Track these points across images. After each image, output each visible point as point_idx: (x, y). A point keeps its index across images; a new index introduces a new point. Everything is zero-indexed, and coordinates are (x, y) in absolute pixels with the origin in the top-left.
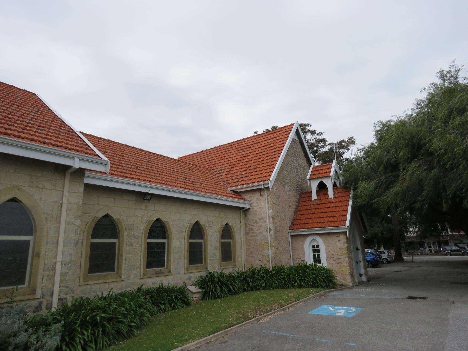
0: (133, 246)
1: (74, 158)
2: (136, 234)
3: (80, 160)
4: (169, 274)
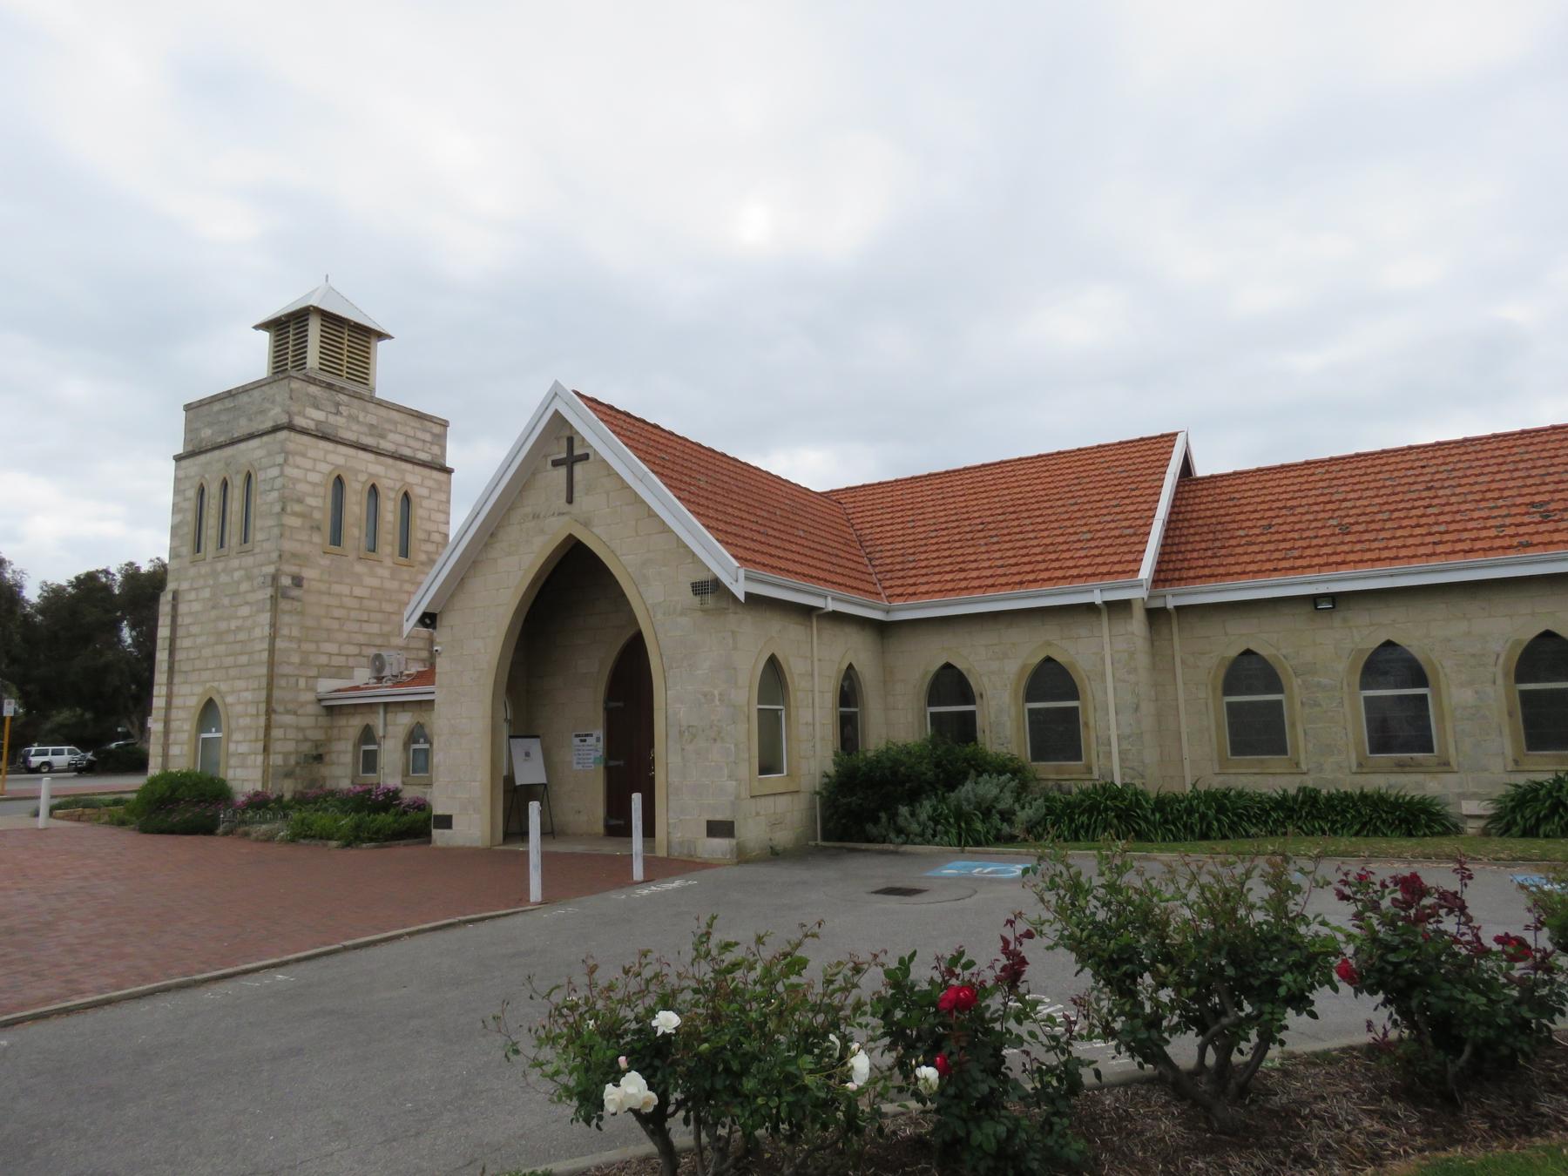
0: (1320, 705)
1: (826, 597)
2: (1324, 681)
3: (833, 599)
4: (1446, 768)
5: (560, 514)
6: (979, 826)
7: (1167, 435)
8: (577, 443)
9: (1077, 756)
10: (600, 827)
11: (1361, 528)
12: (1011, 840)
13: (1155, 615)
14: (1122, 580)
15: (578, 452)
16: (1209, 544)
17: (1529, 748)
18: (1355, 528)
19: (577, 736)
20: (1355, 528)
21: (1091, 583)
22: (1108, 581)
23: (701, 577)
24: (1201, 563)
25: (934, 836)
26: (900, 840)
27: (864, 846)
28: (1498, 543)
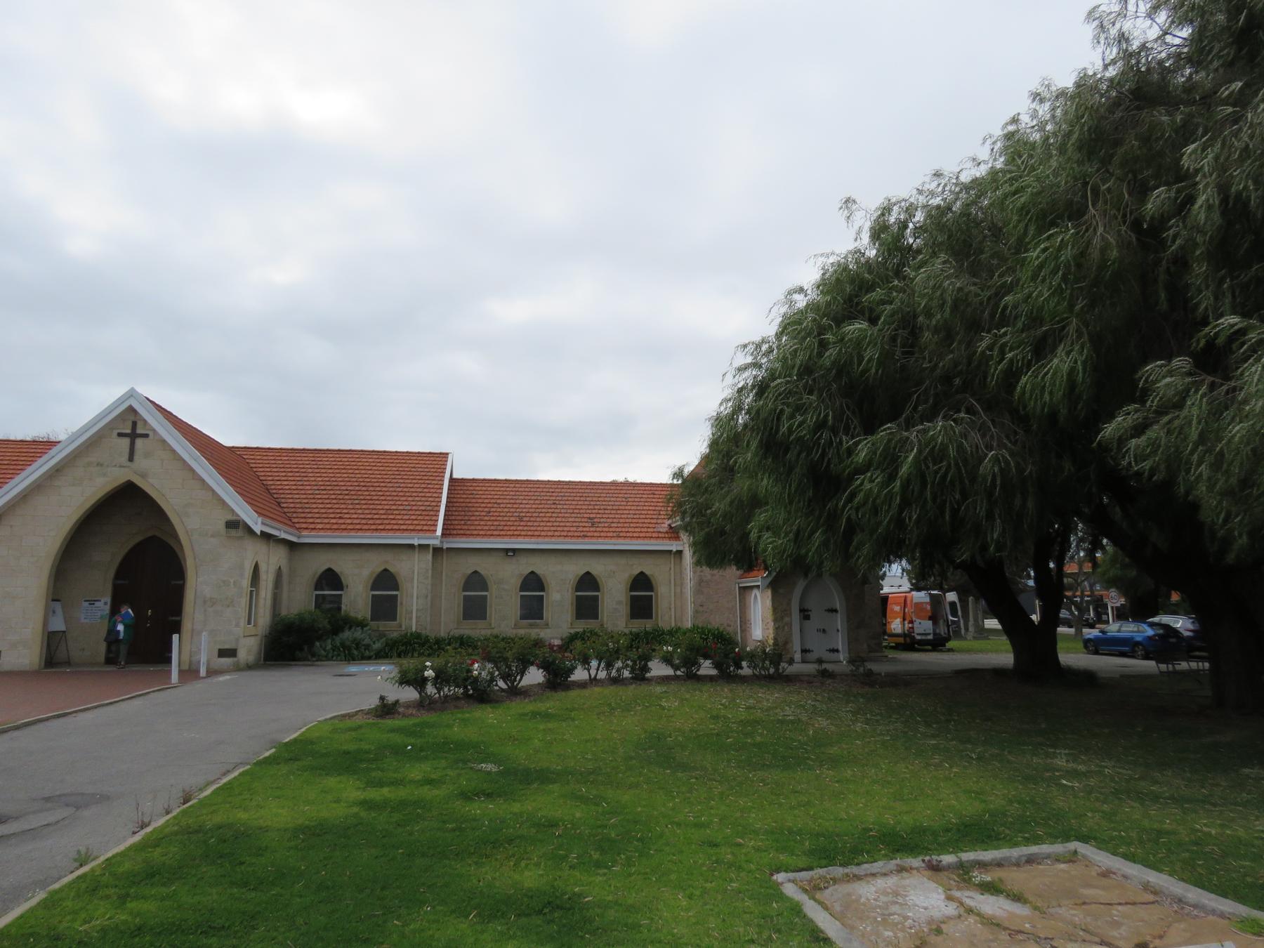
3: (284, 532)
5: (121, 466)
6: (356, 652)
7: (443, 454)
8: (139, 425)
9: (394, 619)
10: (102, 658)
11: (527, 519)
12: (369, 658)
13: (437, 551)
14: (428, 535)
15: (139, 431)
16: (462, 518)
17: (577, 619)
18: (525, 519)
19: (85, 601)
20: (525, 519)
21: (413, 534)
22: (421, 534)
23: (230, 517)
24: (459, 527)
25: (332, 657)
26: (314, 659)
27: (293, 663)
28: (576, 534)
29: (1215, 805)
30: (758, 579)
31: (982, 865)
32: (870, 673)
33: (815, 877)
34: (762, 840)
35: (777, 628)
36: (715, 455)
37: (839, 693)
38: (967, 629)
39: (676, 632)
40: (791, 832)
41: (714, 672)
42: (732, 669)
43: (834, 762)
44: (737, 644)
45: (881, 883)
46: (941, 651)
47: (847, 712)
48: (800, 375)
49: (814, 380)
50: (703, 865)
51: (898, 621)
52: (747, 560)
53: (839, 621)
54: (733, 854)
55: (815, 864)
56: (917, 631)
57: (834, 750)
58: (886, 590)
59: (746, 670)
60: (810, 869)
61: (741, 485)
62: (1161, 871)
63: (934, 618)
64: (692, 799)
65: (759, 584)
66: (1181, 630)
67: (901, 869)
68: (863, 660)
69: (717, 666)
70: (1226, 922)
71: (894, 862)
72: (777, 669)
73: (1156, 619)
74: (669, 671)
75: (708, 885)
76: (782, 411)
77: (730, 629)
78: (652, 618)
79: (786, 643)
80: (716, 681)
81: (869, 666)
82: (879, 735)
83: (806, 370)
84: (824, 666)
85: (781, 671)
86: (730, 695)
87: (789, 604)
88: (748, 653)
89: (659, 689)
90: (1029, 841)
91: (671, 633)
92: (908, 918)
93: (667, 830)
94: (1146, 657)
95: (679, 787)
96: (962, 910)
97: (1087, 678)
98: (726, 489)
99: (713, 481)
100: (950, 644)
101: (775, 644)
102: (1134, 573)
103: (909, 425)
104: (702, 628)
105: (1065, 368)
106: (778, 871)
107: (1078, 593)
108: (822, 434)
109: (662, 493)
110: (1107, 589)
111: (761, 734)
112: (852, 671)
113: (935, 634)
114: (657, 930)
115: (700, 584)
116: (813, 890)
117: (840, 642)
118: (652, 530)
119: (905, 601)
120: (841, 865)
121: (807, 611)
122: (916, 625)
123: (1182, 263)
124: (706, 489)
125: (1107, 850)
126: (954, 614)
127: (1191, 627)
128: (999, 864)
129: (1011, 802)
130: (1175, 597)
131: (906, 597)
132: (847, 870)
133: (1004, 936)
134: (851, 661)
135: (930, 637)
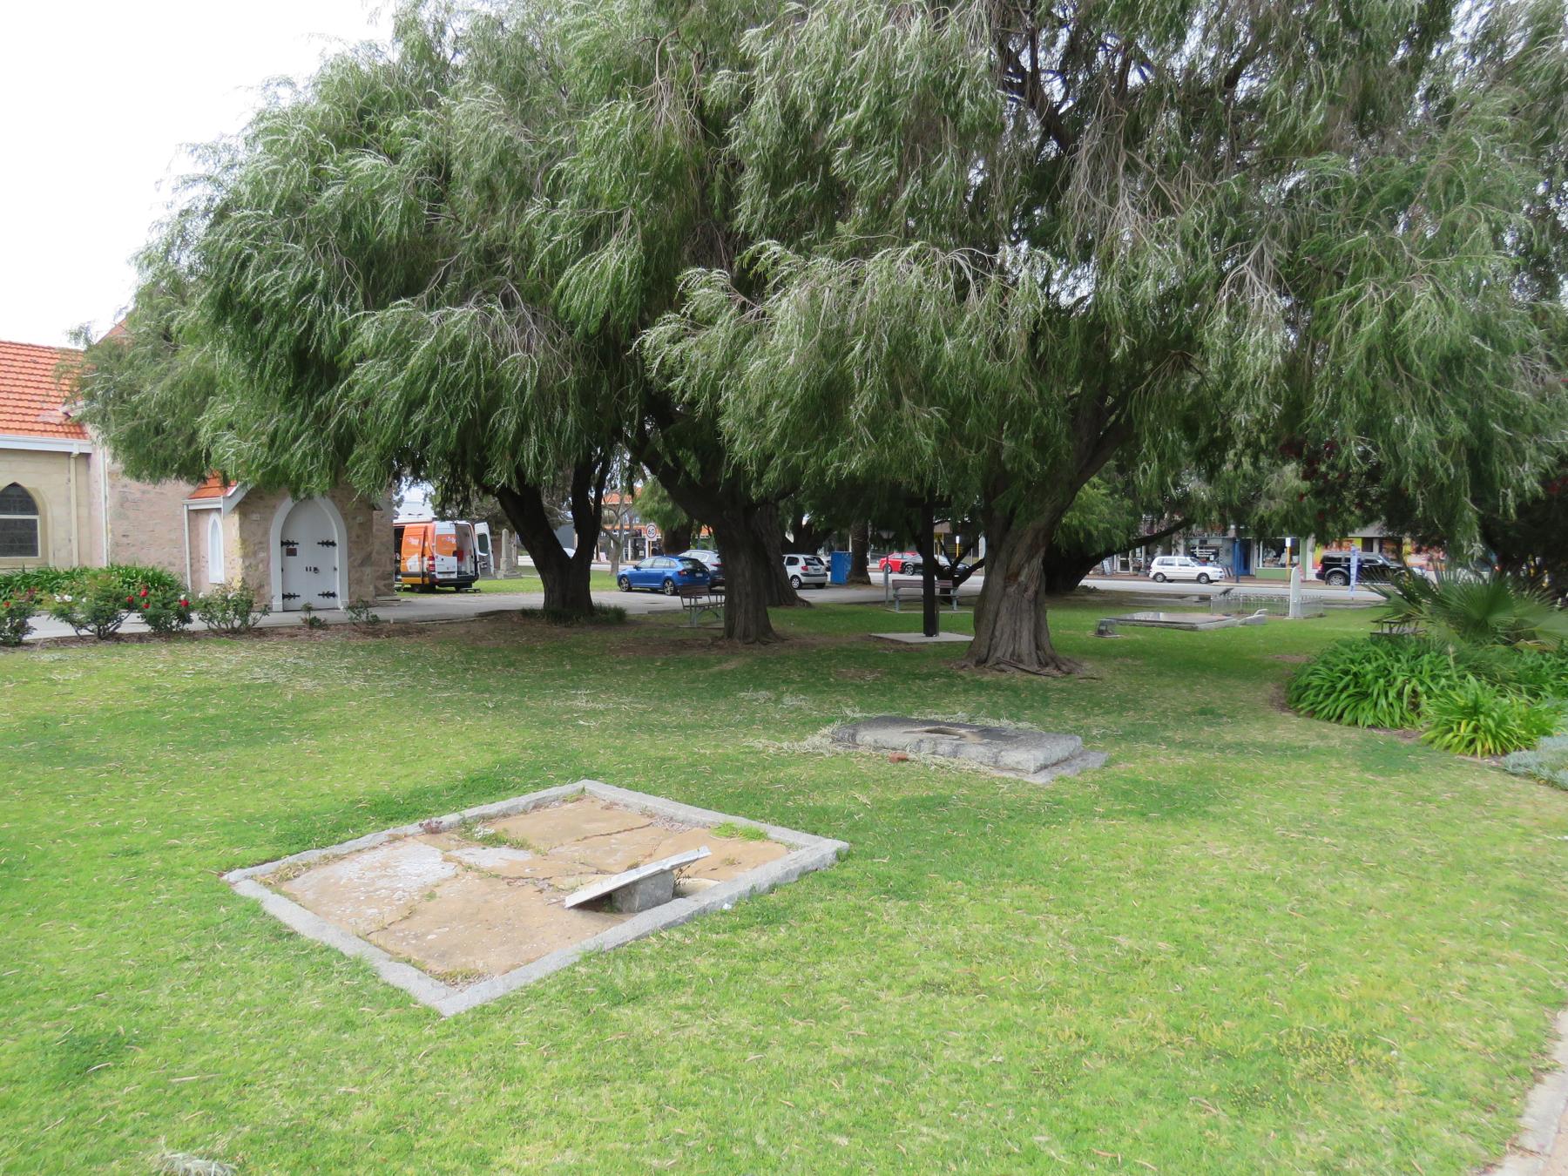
29: (713, 728)
30: (222, 500)
31: (486, 819)
32: (375, 621)
33: (283, 867)
34: (209, 836)
35: (247, 568)
36: (147, 311)
37: (333, 647)
38: (497, 567)
39: (81, 573)
40: (251, 819)
41: (146, 629)
42: (174, 623)
43: (317, 729)
44: (185, 589)
45: (367, 858)
46: (467, 592)
47: (341, 668)
48: (279, 212)
49: (303, 221)
50: (113, 882)
51: (416, 557)
52: (194, 468)
53: (337, 556)
54: (163, 860)
55: (284, 851)
56: (438, 569)
57: (321, 715)
58: (401, 520)
59: (197, 623)
60: (277, 858)
61: (190, 359)
62: (658, 795)
63: (459, 554)
64: (99, 801)
65: (220, 506)
66: (708, 565)
67: (394, 839)
68: (367, 605)
69: (151, 620)
70: (707, 831)
71: (386, 832)
72: (245, 621)
73: (686, 554)
74: (68, 630)
75: (122, 905)
76: (249, 258)
77: (174, 570)
78: (36, 554)
79: (261, 586)
80: (148, 641)
81: (374, 611)
82: (381, 692)
83: (293, 205)
84: (313, 614)
85: (250, 623)
86: (171, 659)
87: (266, 532)
88: (201, 601)
89: (47, 657)
90: (537, 787)
91: (70, 575)
92: (398, 889)
93: (54, 846)
94: (674, 593)
95: (78, 788)
96: (459, 869)
97: (617, 617)
98: (164, 365)
99: (142, 350)
100: (475, 585)
101: (243, 588)
102: (670, 506)
103: (432, 304)
104: (126, 568)
105: (611, 266)
106: (230, 869)
107: (618, 527)
108: (309, 299)
109: (52, 362)
110: (645, 523)
111: (217, 706)
112: (351, 618)
113: (459, 573)
114: (32, 979)
115: (123, 505)
116: (275, 884)
117: (338, 584)
118: (32, 419)
119: (425, 533)
120: (318, 847)
121: (293, 543)
122: (437, 562)
123: (736, 167)
124: (131, 364)
125: (614, 783)
126: (483, 548)
127: (717, 561)
128: (505, 815)
129: (525, 749)
130: (704, 533)
131: (426, 528)
132: (324, 852)
133: (503, 885)
134: (350, 608)
135: (454, 576)
